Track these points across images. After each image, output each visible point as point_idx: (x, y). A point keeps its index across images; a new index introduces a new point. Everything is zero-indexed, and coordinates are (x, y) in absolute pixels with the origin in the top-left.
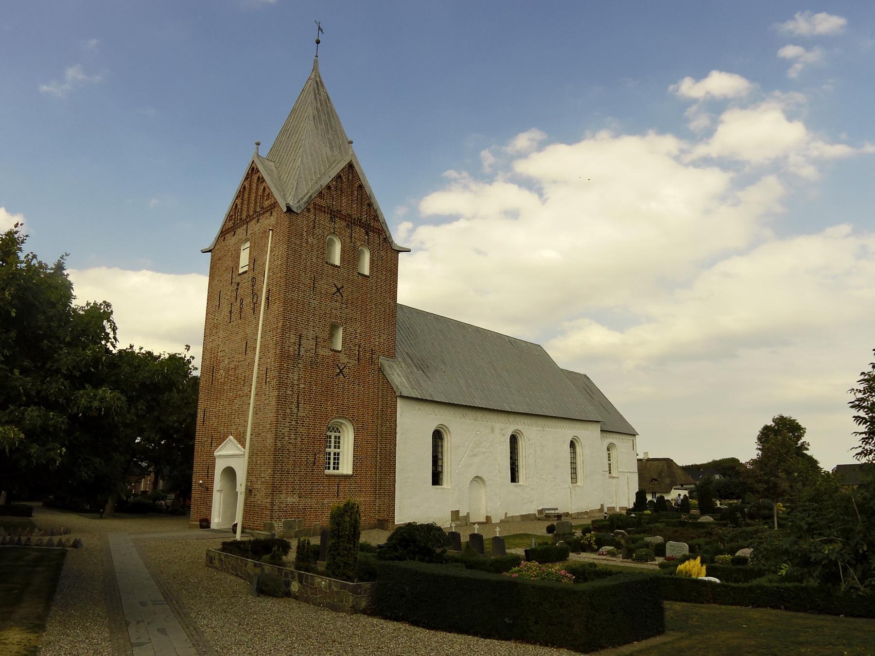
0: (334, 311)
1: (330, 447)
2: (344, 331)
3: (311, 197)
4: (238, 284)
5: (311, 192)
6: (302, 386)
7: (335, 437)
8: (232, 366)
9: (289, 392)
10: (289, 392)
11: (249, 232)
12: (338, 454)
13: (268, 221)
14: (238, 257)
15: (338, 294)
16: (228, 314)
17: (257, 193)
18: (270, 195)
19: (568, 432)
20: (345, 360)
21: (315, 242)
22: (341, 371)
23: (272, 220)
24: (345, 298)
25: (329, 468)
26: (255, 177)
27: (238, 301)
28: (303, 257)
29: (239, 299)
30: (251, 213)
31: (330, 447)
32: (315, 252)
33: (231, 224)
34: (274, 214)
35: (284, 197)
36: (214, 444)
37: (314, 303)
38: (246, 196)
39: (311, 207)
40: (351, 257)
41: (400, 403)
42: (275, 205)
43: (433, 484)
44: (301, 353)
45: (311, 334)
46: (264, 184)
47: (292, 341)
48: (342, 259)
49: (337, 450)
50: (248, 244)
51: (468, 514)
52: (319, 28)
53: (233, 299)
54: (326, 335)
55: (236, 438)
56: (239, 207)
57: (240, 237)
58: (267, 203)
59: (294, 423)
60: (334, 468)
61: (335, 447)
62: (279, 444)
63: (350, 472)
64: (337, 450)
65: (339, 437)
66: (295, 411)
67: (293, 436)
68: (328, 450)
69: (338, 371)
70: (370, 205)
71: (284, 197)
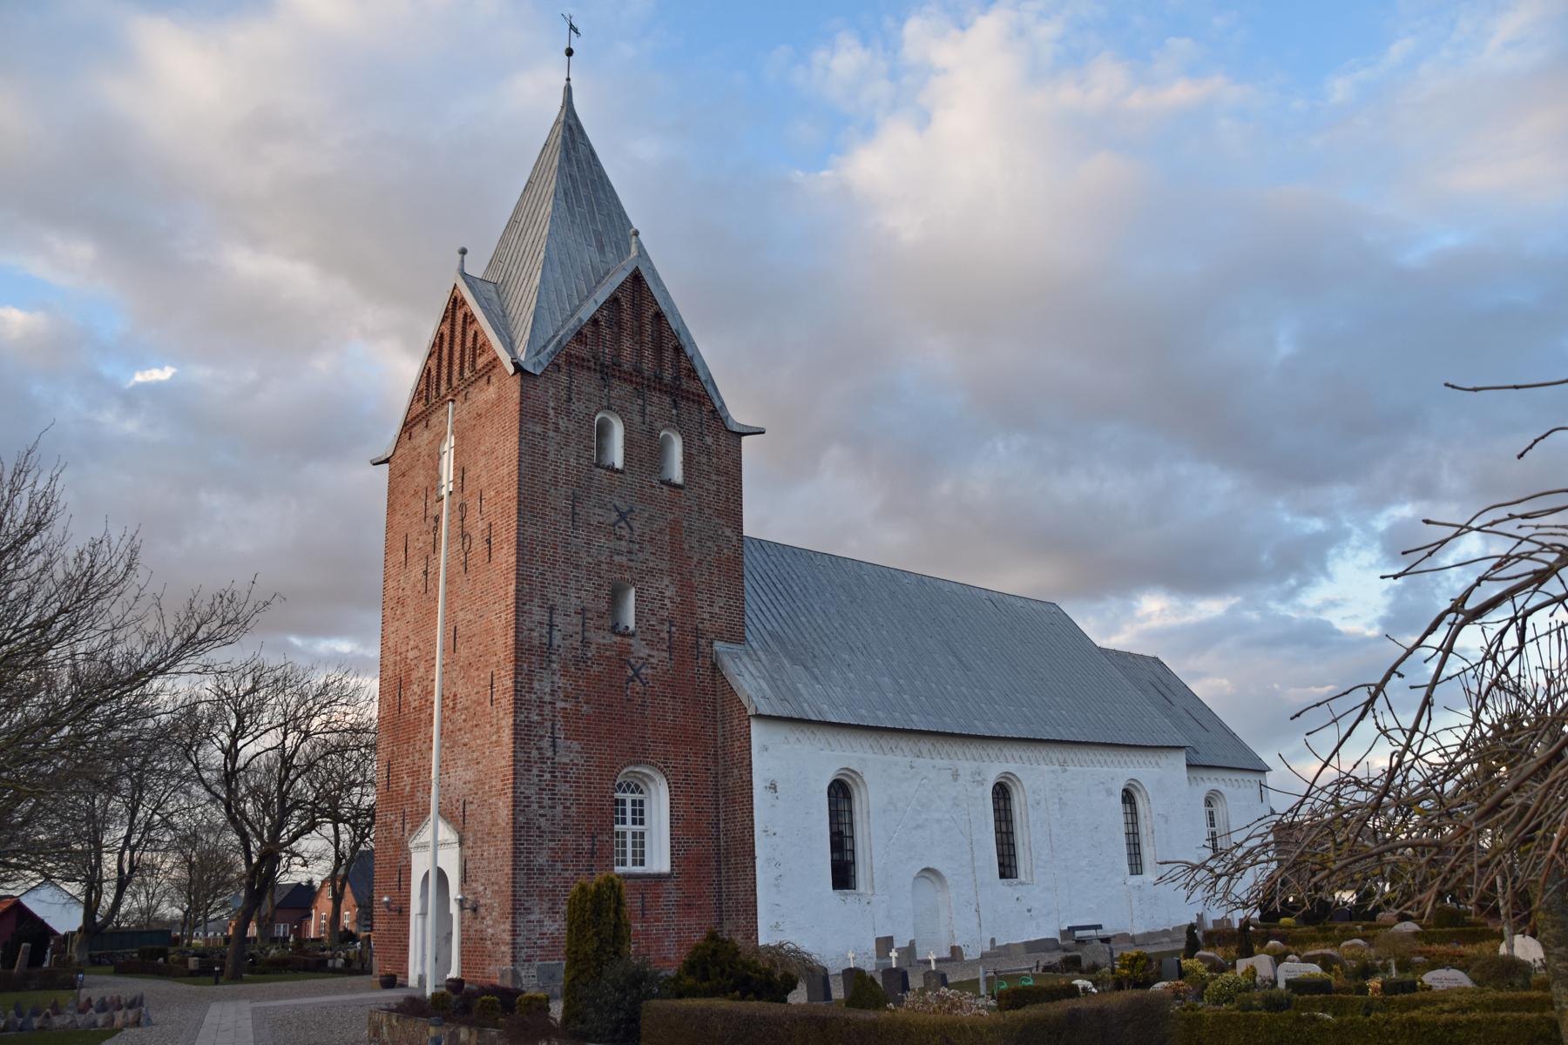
1: (624, 822)
3: (560, 342)
6: (560, 705)
7: (634, 803)
13: (485, 394)
15: (623, 524)
16: (420, 575)
21: (571, 428)
23: (491, 392)
25: (624, 863)
28: (551, 456)
31: (624, 822)
33: (420, 407)
34: (493, 379)
39: (561, 361)
40: (646, 451)
41: (757, 731)
43: (1002, 876)
44: (556, 642)
46: (474, 327)
47: (537, 618)
49: (638, 828)
51: (912, 943)
54: (603, 605)
56: (434, 373)
59: (547, 776)
63: (665, 867)
65: (641, 803)
66: (549, 754)
67: (547, 802)
70: (679, 349)
71: (510, 347)
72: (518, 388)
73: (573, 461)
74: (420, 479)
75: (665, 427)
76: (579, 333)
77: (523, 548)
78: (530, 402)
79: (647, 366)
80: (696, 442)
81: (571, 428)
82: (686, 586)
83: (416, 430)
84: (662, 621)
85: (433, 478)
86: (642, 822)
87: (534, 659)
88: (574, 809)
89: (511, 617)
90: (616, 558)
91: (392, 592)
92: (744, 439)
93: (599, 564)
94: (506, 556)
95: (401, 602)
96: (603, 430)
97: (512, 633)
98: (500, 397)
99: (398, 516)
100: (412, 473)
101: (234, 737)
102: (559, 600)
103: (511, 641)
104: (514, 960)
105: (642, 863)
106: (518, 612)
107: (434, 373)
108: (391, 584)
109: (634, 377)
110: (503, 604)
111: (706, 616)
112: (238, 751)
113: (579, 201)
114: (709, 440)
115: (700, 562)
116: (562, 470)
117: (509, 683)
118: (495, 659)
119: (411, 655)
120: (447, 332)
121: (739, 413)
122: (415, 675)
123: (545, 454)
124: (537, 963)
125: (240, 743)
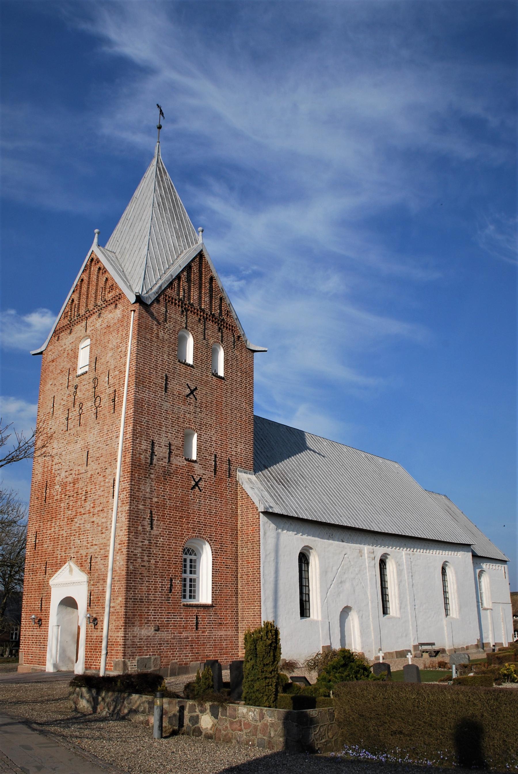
0: (188, 416)
2: (199, 439)
3: (160, 287)
5: (160, 282)
6: (155, 500)
8: (70, 479)
9: (141, 507)
10: (141, 507)
11: (89, 329)
12: (195, 580)
13: (112, 315)
14: (76, 357)
15: (192, 396)
18: (113, 287)
19: (438, 556)
22: (197, 484)
23: (118, 313)
24: (199, 401)
25: (185, 597)
26: (94, 269)
27: (77, 405)
28: (154, 353)
29: (77, 404)
30: (91, 307)
32: (166, 349)
33: (66, 322)
34: (119, 306)
35: (130, 287)
36: (49, 571)
37: (166, 405)
38: (84, 289)
40: (205, 354)
42: (120, 296)
43: (301, 616)
44: (155, 461)
45: (164, 441)
46: (106, 275)
47: (143, 447)
48: (195, 357)
50: (88, 342)
53: (71, 404)
55: (76, 563)
56: (76, 302)
57: (78, 335)
58: (109, 296)
59: (146, 542)
60: (190, 597)
62: (131, 567)
63: (209, 602)
66: (148, 529)
67: (146, 558)
68: (184, 576)
69: (193, 483)
71: (130, 287)
94: (124, 410)
97: (129, 455)
113: (165, 210)
124: (137, 658)
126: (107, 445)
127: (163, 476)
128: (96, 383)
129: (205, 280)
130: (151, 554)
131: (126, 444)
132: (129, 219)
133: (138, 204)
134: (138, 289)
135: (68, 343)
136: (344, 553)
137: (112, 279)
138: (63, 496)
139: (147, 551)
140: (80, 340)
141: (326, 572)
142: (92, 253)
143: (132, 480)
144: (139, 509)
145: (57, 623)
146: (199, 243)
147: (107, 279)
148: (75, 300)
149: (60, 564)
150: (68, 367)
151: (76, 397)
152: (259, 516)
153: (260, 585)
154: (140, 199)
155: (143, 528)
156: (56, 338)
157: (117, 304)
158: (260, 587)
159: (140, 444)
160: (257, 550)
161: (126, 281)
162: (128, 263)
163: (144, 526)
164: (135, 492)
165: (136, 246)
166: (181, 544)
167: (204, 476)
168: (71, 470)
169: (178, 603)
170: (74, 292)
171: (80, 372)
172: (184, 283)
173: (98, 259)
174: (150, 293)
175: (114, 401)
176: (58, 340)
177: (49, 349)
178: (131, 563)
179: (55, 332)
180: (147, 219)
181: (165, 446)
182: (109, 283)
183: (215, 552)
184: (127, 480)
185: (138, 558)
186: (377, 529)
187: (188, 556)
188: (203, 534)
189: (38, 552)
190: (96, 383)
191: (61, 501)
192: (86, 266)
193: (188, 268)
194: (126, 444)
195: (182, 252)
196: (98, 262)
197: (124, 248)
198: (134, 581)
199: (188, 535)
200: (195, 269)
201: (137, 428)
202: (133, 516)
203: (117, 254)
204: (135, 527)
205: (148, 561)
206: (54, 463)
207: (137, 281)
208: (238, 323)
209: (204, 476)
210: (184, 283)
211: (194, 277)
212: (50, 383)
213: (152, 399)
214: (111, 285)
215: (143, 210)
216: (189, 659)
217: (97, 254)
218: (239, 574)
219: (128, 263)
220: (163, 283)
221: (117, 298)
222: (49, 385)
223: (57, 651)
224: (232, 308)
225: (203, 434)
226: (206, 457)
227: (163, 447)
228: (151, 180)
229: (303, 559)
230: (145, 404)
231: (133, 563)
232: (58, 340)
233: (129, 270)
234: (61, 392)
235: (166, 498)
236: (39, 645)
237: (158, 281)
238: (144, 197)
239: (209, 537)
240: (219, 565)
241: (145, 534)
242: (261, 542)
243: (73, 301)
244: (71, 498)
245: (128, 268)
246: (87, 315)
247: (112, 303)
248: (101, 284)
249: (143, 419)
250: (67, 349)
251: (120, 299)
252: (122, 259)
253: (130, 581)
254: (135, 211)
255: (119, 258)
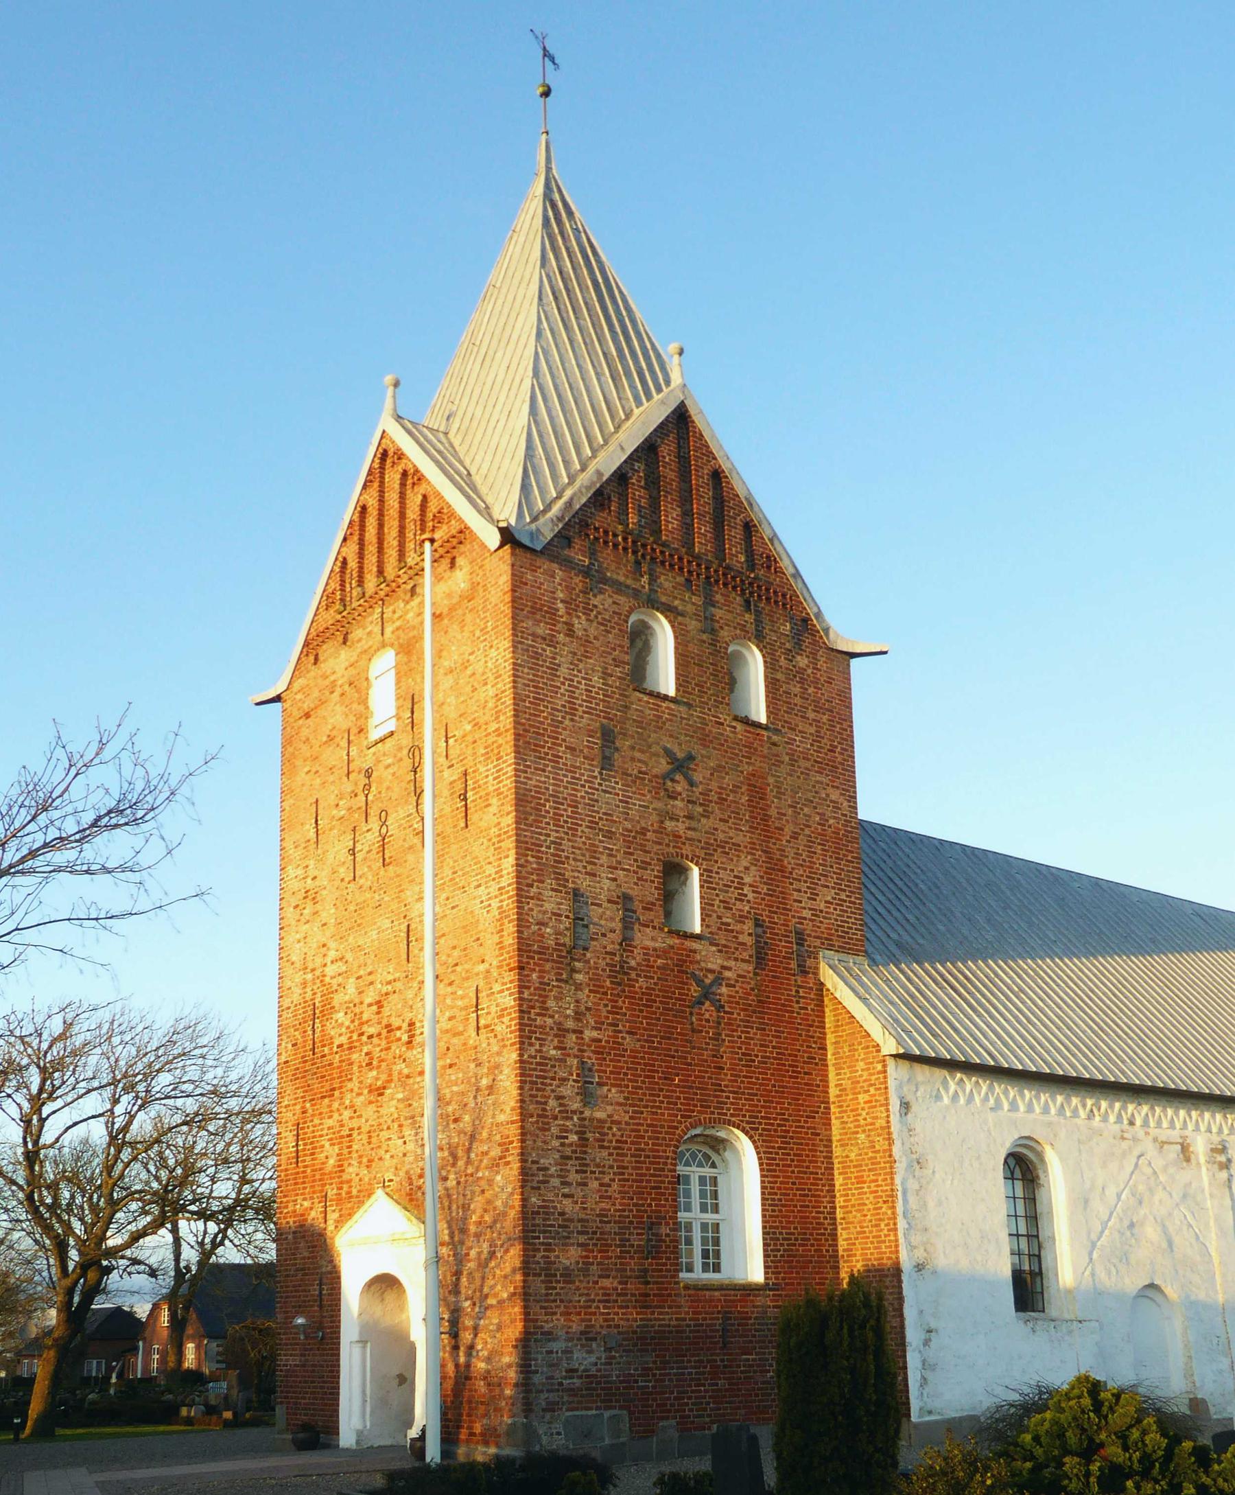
3: (569, 504)
4: (368, 774)
5: (568, 493)
6: (589, 1034)
7: (702, 1180)
16: (344, 855)
17: (402, 515)
20: (715, 962)
21: (592, 631)
26: (393, 478)
28: (563, 671)
29: (373, 812)
33: (330, 617)
34: (460, 561)
40: (709, 671)
42: (463, 535)
43: (1017, 1310)
46: (422, 489)
49: (710, 1217)
52: (546, 54)
54: (652, 893)
56: (353, 564)
59: (574, 1138)
61: (704, 1209)
64: (710, 1217)
65: (714, 1181)
67: (573, 1177)
70: (749, 528)
71: (486, 512)
72: (508, 569)
73: (596, 680)
74: (336, 717)
75: (735, 638)
76: (599, 493)
77: (527, 805)
78: (526, 590)
79: (702, 543)
80: (783, 662)
81: (592, 631)
82: (775, 870)
83: (327, 650)
84: (742, 919)
85: (359, 716)
86: (716, 1209)
87: (548, 966)
88: (615, 1186)
89: (509, 904)
90: (669, 824)
91: (295, 885)
92: (854, 662)
93: (643, 832)
94: (497, 817)
95: (311, 896)
96: (640, 639)
97: (510, 928)
98: (474, 586)
99: (301, 776)
100: (321, 712)
101: (37, 1102)
102: (584, 883)
103: (510, 941)
104: (528, 1409)
105: (717, 1268)
106: (522, 895)
107: (353, 564)
108: (291, 871)
109: (682, 561)
110: (493, 889)
111: (806, 914)
112: (42, 1121)
114: (802, 661)
115: (795, 836)
116: (580, 693)
117: (509, 1001)
118: (482, 967)
119: (331, 970)
120: (372, 503)
121: (844, 624)
122: (338, 999)
123: (554, 668)
125: (46, 1111)
126: (453, 908)
127: (609, 977)
128: (417, 759)
129: (700, 479)
130: (587, 1165)
131: (501, 901)
132: (478, 343)
133: (500, 302)
134: (507, 513)
135: (340, 670)
136: (1136, 1153)
137: (438, 495)
138: (355, 1037)
139: (577, 1158)
140: (369, 655)
141: (1086, 1201)
142: (382, 438)
143: (521, 988)
144: (545, 1058)
145: (361, 1333)
146: (673, 385)
147: (425, 497)
148: (349, 560)
149: (358, 1197)
150: (345, 727)
151: (370, 797)
152: (885, 1066)
153: (896, 1235)
154: (504, 291)
155: (561, 1105)
156: (312, 658)
157: (454, 558)
158: (897, 1240)
159: (539, 899)
160: (884, 1151)
161: (468, 486)
162: (481, 453)
163: (563, 1097)
164: (533, 1016)
165: (498, 407)
166: (671, 1140)
167: (727, 974)
168: (370, 973)
169: (670, 1283)
170: (345, 540)
171: (374, 735)
172: (637, 492)
173: (399, 449)
174: (542, 520)
175: (465, 799)
176: (315, 663)
177: (296, 686)
178: (533, 1188)
179: (306, 644)
180: (524, 336)
181: (609, 901)
182: (433, 508)
183: (768, 1159)
184: (508, 989)
185: (552, 1176)
186: (432, 464)
187: (694, 1168)
188: (732, 1115)
189: (304, 1172)
190: (417, 759)
191: (350, 1048)
192: (370, 472)
193: (648, 450)
194: (501, 901)
195: (628, 416)
196: (399, 458)
197: (469, 415)
198: (545, 1232)
199: (690, 1117)
200: (667, 452)
201: (527, 861)
202: (531, 1076)
203: (451, 436)
204: (537, 1102)
205: (579, 1184)
206: (328, 960)
207: (503, 494)
208: (800, 585)
209: (727, 974)
210: (637, 492)
211: (669, 472)
212: (306, 769)
213: (566, 788)
214: (435, 510)
215: (513, 315)
216: (709, 1416)
217: (394, 438)
218: (838, 1210)
219: (481, 453)
220: (574, 495)
221: (455, 541)
222: (303, 775)
223: (365, 1401)
224: (779, 549)
225: (715, 869)
226: (729, 925)
227: (605, 904)
228: (531, 237)
229: (1023, 1168)
230: (548, 801)
231: (539, 1188)
232: (315, 663)
233: (484, 471)
234: (332, 788)
235: (620, 1027)
236: (322, 1387)
237: (567, 488)
238: (516, 282)
239: (748, 1123)
240: (779, 1188)
241: (567, 1118)
242: (892, 1129)
243: (345, 562)
244: (375, 1040)
245: (478, 465)
246: (382, 593)
247: (441, 557)
248: (413, 513)
249: (542, 838)
250: (339, 683)
251: (461, 543)
252: (465, 446)
253: (534, 1231)
254: (493, 321)
255: (456, 444)
